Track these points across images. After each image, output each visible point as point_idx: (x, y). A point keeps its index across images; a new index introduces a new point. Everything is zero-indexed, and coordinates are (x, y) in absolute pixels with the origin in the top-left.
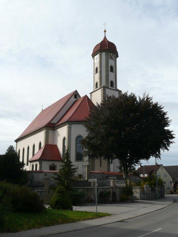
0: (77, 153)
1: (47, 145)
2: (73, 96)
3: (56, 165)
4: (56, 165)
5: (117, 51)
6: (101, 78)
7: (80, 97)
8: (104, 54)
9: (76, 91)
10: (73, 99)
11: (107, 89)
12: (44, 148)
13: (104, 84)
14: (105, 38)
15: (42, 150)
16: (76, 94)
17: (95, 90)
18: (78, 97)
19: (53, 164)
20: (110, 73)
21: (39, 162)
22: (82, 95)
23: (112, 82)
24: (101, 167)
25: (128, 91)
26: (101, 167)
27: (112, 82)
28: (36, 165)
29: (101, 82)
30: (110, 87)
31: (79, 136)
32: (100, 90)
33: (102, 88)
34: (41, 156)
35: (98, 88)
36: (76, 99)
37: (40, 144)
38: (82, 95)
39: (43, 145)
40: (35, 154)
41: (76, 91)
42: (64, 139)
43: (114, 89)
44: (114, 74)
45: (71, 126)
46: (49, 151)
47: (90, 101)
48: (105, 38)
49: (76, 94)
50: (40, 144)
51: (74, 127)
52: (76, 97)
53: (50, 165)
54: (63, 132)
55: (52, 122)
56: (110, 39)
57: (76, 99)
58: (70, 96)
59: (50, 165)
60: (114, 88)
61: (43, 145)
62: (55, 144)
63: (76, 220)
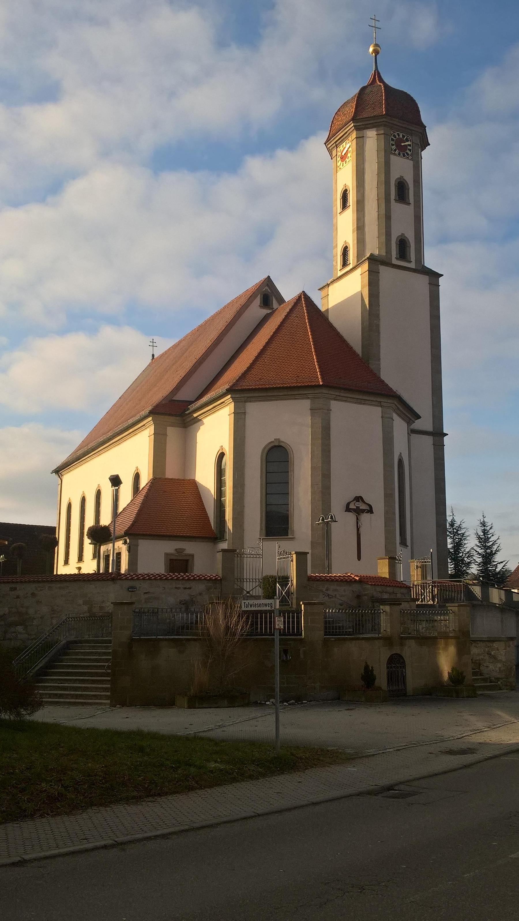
0: (267, 512)
1: (154, 483)
2: (258, 301)
3: (192, 556)
4: (192, 556)
5: (422, 123)
6: (360, 228)
7: (281, 300)
8: (371, 134)
9: (268, 282)
10: (257, 311)
11: (384, 270)
12: (145, 491)
13: (373, 247)
14: (377, 75)
15: (140, 498)
16: (267, 294)
17: (340, 274)
18: (275, 304)
19: (179, 551)
20: (397, 208)
21: (125, 543)
22: (288, 292)
23: (403, 243)
24: (359, 558)
25: (483, 524)
26: (359, 558)
27: (403, 243)
28: (66, 562)
29: (361, 241)
30: (395, 262)
31: (275, 446)
32: (359, 271)
33: (366, 266)
34: (132, 525)
35: (351, 267)
36: (269, 311)
37: (137, 477)
38: (288, 292)
39: (144, 482)
40: (120, 510)
41: (268, 282)
42: (221, 455)
43: (412, 265)
44: (408, 210)
45: (245, 407)
46: (165, 508)
47: (318, 318)
48: (377, 75)
49: (267, 294)
50: (137, 477)
51: (255, 409)
52: (266, 302)
53: (166, 554)
54: (215, 431)
55: (179, 397)
56: (392, 81)
57: (269, 311)
58: (243, 301)
59: (166, 554)
60: (410, 262)
61: (144, 482)
62: (188, 478)
63: (443, 554)
